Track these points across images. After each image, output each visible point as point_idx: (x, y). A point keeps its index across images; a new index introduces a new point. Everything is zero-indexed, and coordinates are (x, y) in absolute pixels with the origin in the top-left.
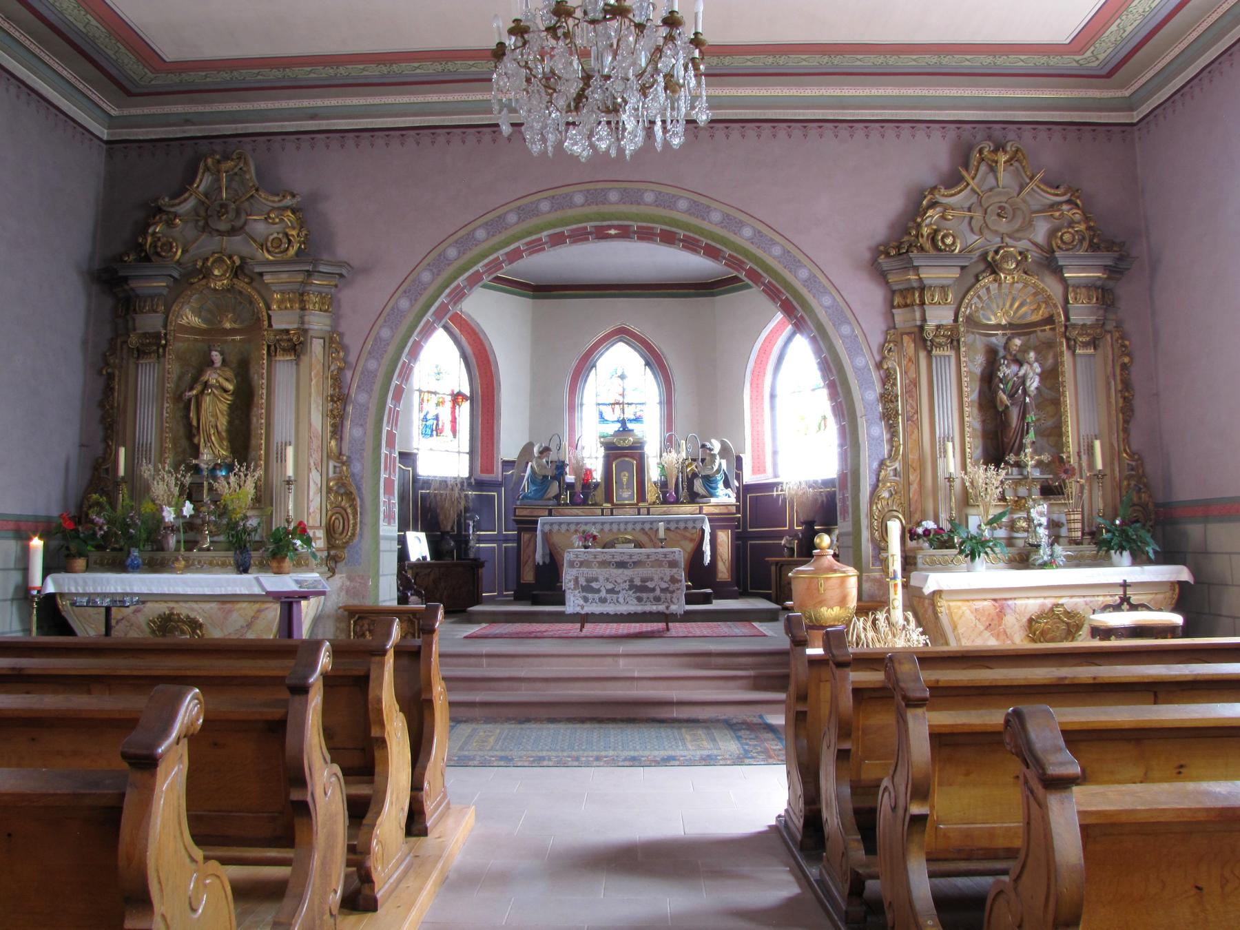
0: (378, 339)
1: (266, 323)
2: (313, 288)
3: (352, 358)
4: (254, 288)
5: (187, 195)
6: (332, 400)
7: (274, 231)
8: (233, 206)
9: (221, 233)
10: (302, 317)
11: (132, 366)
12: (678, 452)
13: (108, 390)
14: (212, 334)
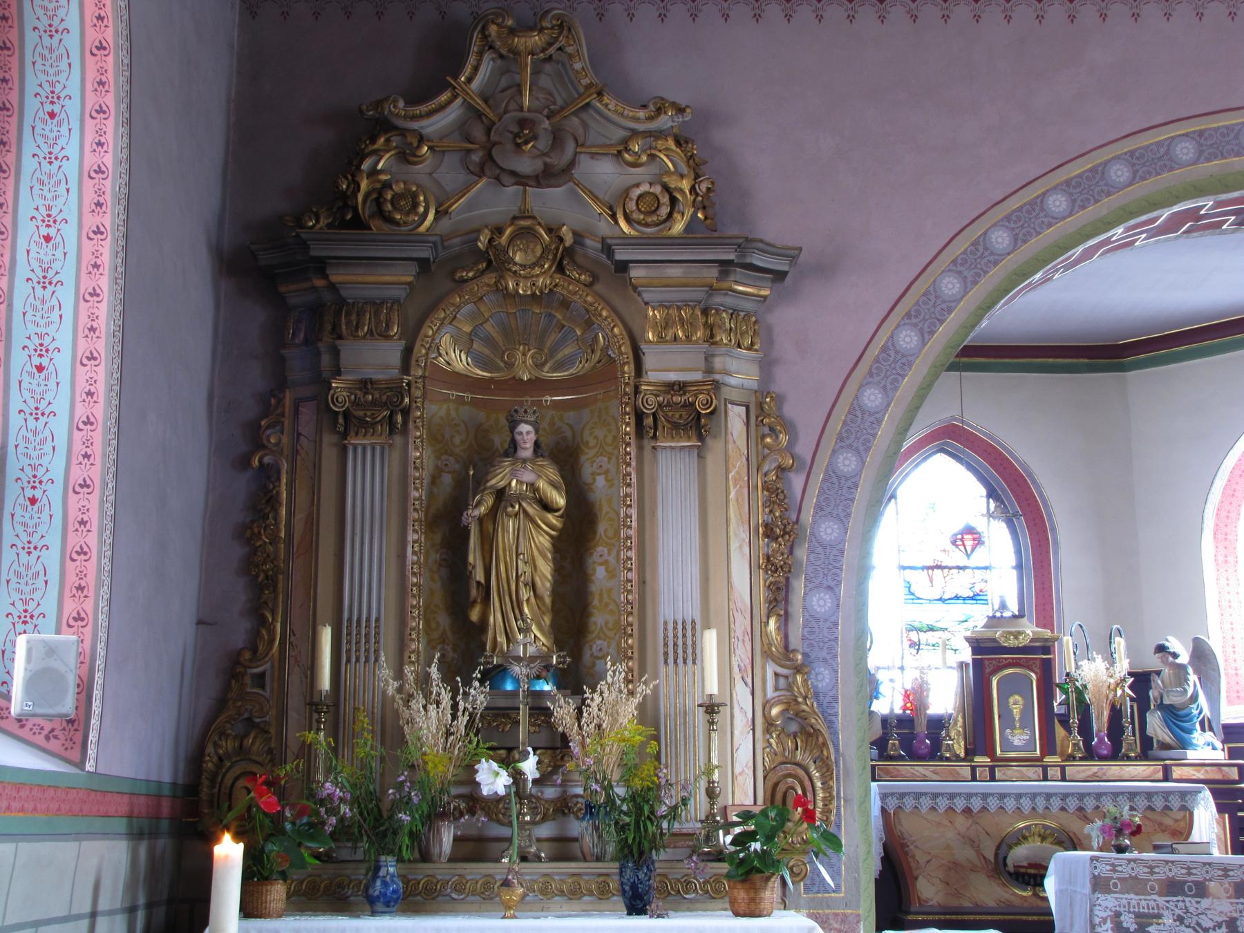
0: (856, 410)
1: (629, 369)
2: (729, 301)
3: (804, 448)
4: (598, 295)
5: (444, 97)
6: (766, 535)
7: (642, 180)
8: (546, 124)
9: (521, 180)
10: (708, 358)
11: (329, 455)
12: (1111, 659)
13: (263, 502)
14: (502, 395)
